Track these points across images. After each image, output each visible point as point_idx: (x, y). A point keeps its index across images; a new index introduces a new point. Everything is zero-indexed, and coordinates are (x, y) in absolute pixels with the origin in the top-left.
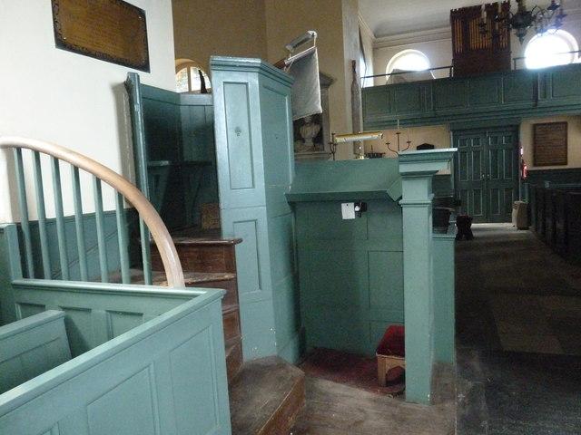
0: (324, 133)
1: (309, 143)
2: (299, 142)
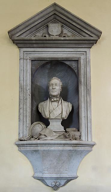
0: (83, 114)
1: (56, 126)
2: (39, 127)
